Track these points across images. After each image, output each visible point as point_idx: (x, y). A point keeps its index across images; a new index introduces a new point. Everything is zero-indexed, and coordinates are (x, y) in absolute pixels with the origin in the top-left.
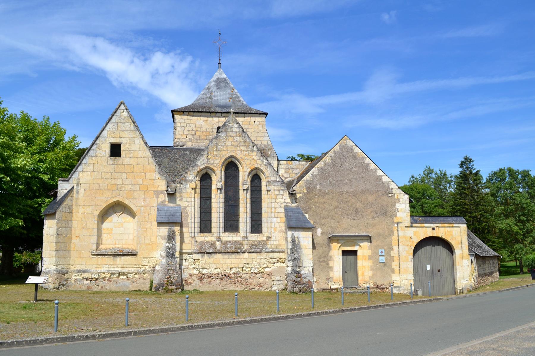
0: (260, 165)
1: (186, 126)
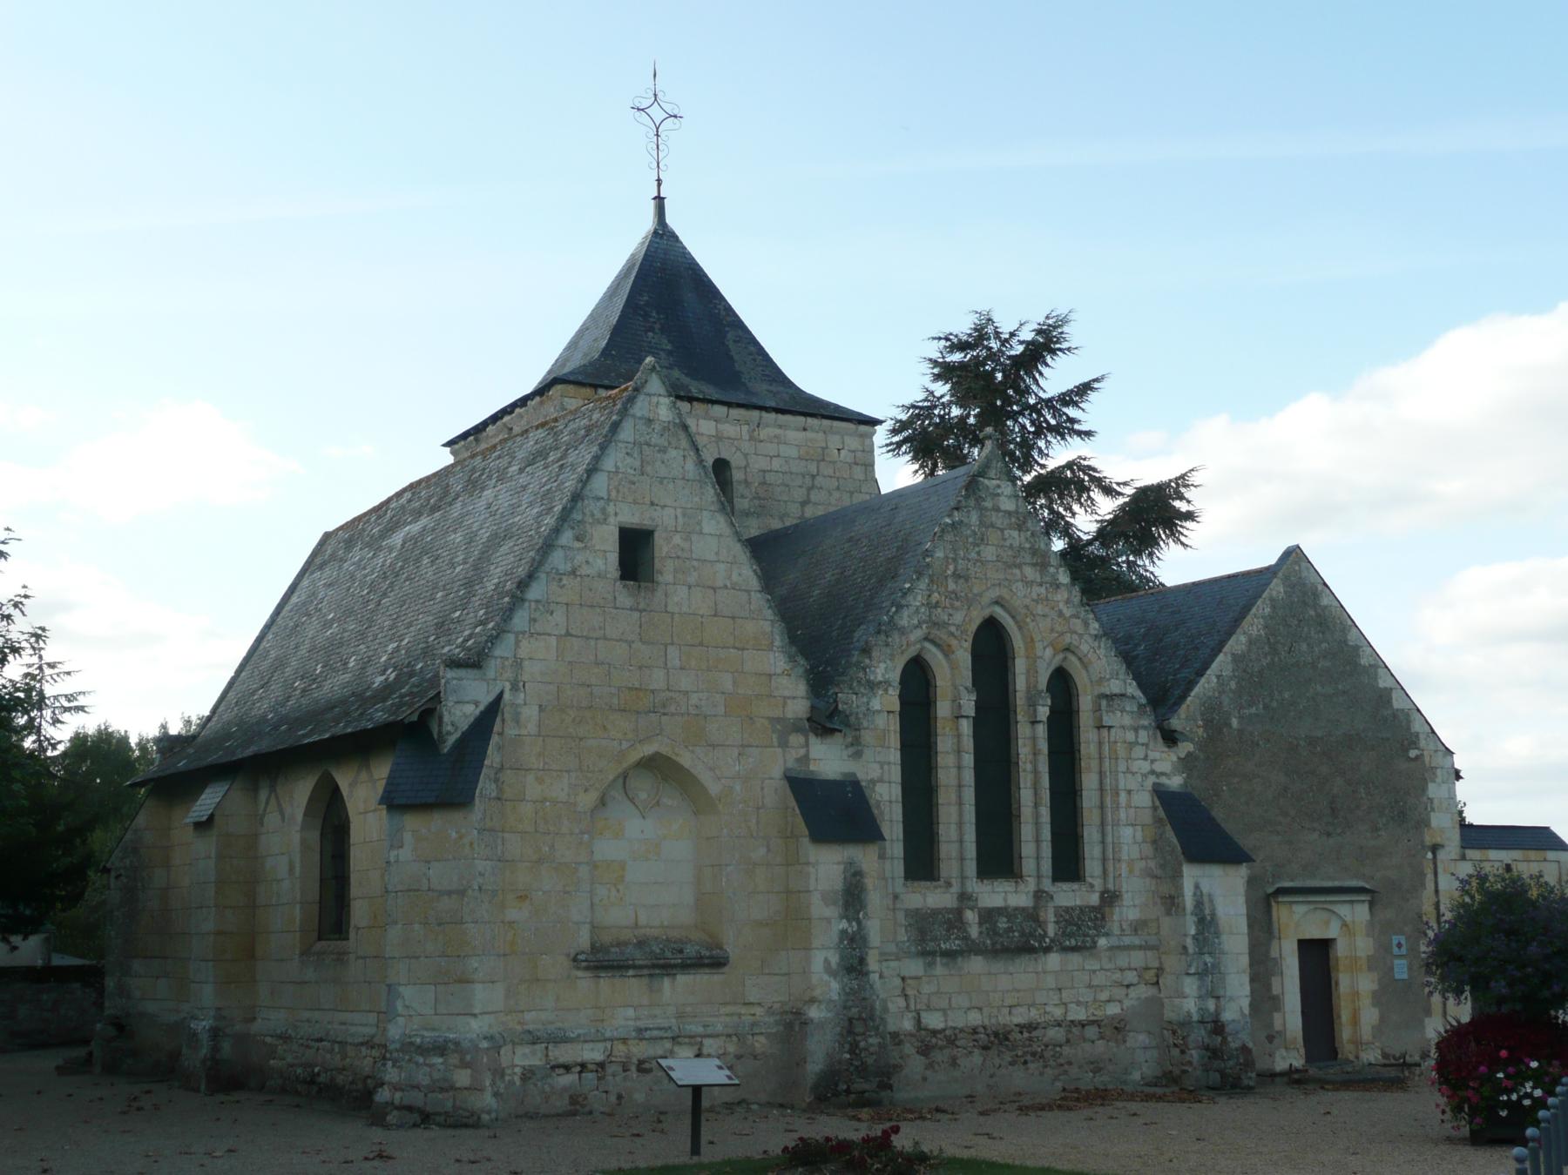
0: (1081, 636)
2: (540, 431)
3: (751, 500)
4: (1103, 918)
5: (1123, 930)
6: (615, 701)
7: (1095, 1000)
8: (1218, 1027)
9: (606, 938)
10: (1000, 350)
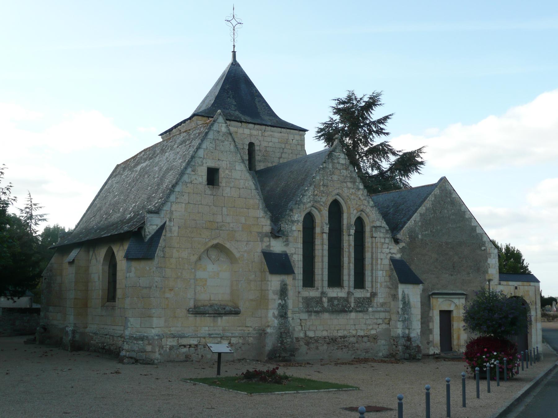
0: (366, 206)
2: (185, 133)
4: (371, 301)
5: (377, 305)
6: (204, 225)
7: (367, 329)
8: (409, 339)
9: (199, 304)
10: (357, 104)
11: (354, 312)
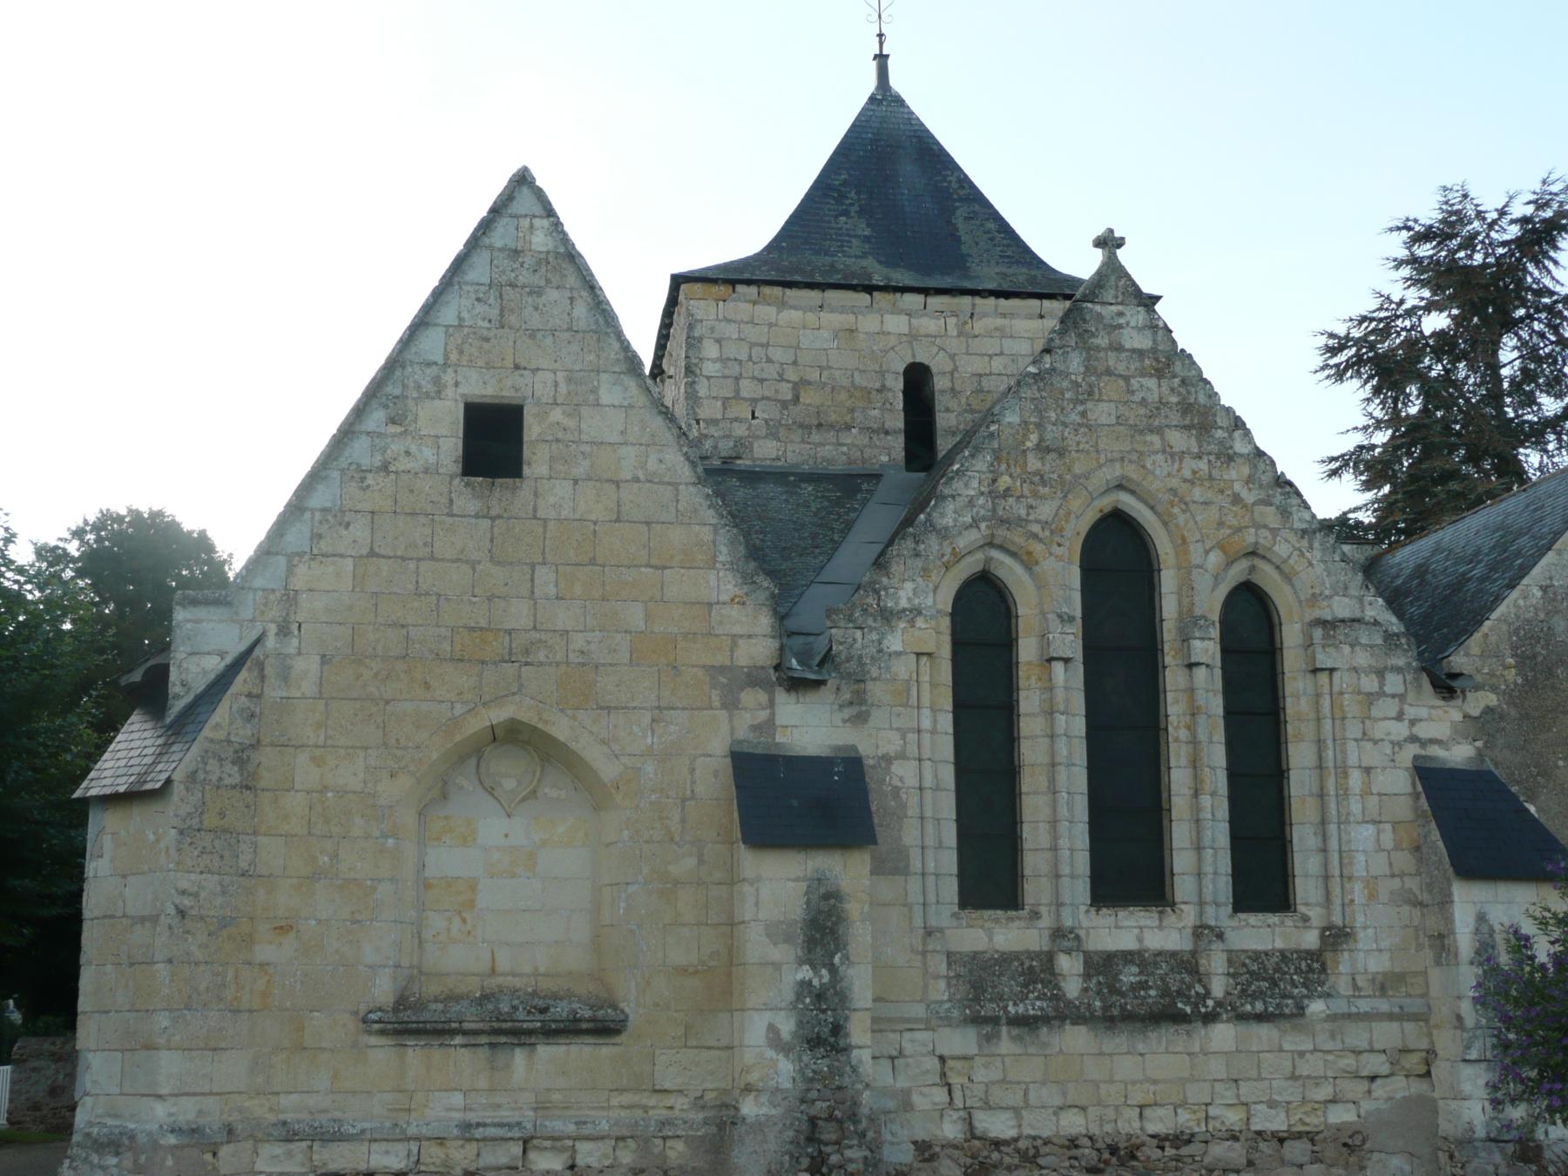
0: (1274, 532)
1: (750, 358)
3: (959, 414)
4: (1324, 969)
5: (1356, 987)
11: (1228, 1021)
